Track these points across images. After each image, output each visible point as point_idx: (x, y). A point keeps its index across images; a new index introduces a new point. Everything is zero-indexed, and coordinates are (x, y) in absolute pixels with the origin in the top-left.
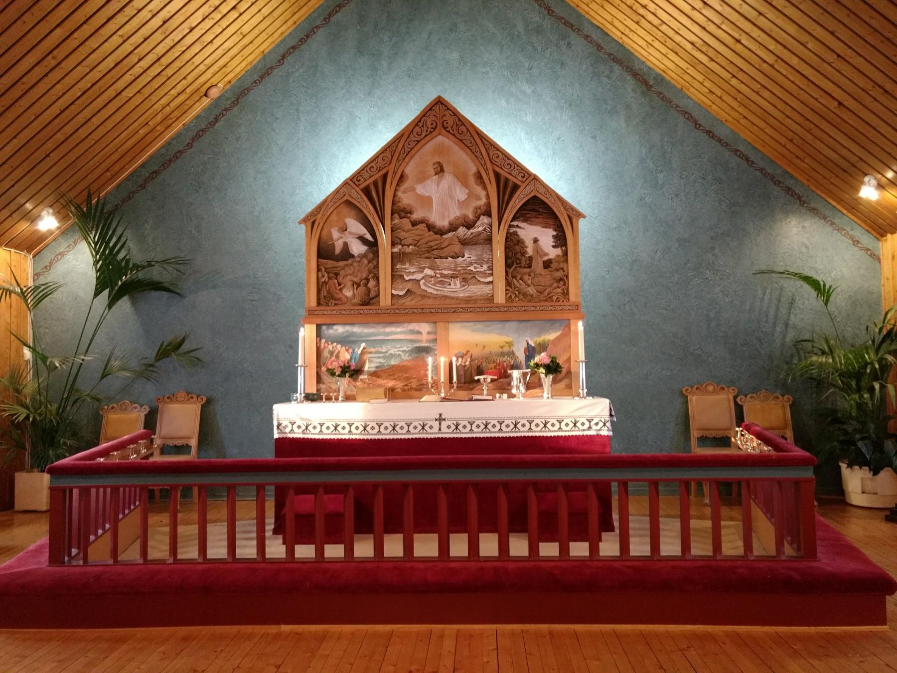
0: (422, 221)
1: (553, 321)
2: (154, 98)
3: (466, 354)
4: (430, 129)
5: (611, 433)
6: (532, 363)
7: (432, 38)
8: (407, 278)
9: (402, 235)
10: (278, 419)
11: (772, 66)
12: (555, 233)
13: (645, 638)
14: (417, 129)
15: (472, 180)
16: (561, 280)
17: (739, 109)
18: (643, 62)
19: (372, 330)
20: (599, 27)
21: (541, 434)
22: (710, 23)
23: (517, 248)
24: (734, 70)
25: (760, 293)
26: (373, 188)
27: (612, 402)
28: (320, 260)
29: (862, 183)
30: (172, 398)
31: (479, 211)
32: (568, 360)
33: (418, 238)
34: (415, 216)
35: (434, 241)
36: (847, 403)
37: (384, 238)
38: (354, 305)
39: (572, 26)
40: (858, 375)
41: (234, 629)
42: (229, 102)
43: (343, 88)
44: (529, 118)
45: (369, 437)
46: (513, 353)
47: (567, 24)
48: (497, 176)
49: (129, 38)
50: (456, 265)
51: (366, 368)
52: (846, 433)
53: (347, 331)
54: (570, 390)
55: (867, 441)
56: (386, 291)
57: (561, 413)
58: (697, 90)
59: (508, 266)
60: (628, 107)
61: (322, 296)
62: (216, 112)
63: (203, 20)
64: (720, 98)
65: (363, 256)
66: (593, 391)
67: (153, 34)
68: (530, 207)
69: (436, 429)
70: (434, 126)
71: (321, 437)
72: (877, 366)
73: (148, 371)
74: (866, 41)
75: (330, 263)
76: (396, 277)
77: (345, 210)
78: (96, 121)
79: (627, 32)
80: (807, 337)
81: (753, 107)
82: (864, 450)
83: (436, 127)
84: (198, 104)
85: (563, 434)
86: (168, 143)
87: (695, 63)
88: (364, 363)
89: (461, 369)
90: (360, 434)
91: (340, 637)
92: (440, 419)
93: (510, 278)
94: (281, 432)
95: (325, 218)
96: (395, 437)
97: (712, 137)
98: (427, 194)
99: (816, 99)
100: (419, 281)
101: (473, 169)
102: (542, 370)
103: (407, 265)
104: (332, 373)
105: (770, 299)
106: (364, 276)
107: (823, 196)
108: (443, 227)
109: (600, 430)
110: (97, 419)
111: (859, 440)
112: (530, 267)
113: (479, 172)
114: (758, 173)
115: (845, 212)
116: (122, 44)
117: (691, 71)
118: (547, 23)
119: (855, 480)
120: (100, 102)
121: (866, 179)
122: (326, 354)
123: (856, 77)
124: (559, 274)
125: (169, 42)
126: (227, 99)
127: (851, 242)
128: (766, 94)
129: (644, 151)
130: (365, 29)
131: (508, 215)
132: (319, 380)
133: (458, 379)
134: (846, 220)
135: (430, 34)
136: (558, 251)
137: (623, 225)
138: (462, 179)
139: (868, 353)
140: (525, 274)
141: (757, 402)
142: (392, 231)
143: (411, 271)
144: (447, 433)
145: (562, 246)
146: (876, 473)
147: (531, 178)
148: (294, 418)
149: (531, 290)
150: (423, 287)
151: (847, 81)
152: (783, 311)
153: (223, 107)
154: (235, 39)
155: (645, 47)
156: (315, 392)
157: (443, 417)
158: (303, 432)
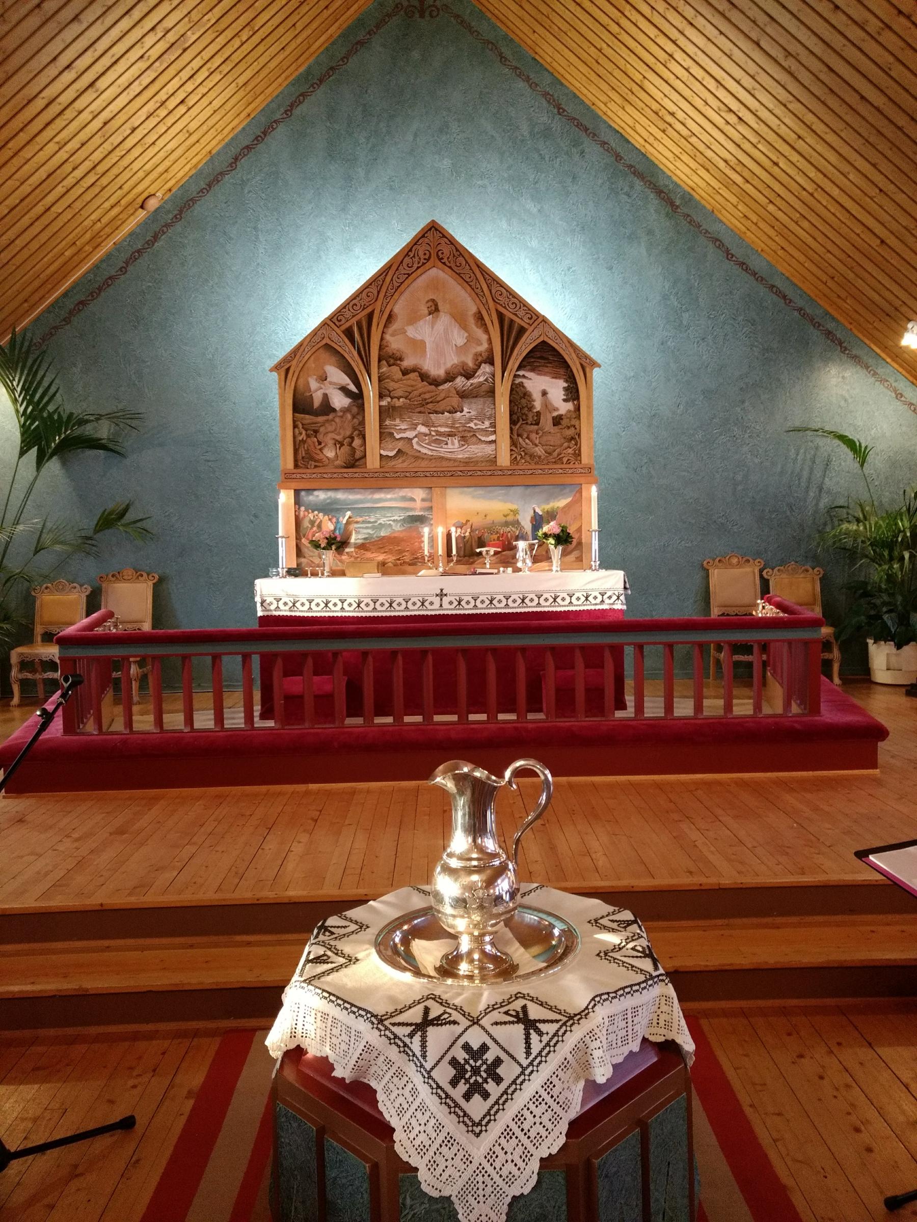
0: (414, 370)
1: (563, 486)
2: (84, 213)
3: (466, 524)
4: (422, 261)
5: (625, 607)
6: (540, 533)
7: (418, 139)
8: (398, 437)
9: (391, 385)
10: (261, 596)
11: (812, 195)
12: (566, 385)
13: (658, 786)
14: (407, 260)
15: (471, 321)
16: (572, 438)
17: (777, 239)
18: (669, 177)
19: (358, 497)
20: (618, 132)
21: (551, 609)
22: (745, 140)
23: (523, 401)
24: (772, 196)
25: (792, 453)
26: (357, 329)
27: (627, 575)
28: (297, 415)
29: (906, 329)
30: (117, 576)
31: (480, 359)
32: (579, 530)
33: (409, 389)
34: (406, 363)
35: (428, 394)
36: (876, 574)
37: (371, 391)
38: (336, 467)
39: (586, 130)
40: (890, 545)
41: (263, 788)
42: (171, 216)
43: (310, 202)
44: (534, 243)
45: (364, 614)
46: (518, 522)
47: (579, 125)
48: (501, 317)
49: (65, 144)
50: (454, 422)
51: (352, 540)
52: (875, 606)
53: (330, 498)
54: (580, 563)
55: (893, 615)
56: (374, 451)
57: (571, 587)
58: (731, 214)
59: (513, 422)
60: (650, 232)
61: (300, 457)
62: (156, 227)
63: (147, 119)
64: (756, 224)
65: (346, 410)
66: (606, 564)
67: (91, 138)
68: (538, 354)
69: (437, 605)
70: (427, 257)
71: (310, 614)
72: (908, 534)
73: (87, 544)
74: (908, 177)
75: (308, 418)
76: (385, 435)
77: (324, 355)
78: (19, 243)
79: (651, 140)
80: (841, 502)
81: (792, 238)
82: (889, 623)
83: (430, 257)
84: (132, 217)
85: (574, 608)
86: (96, 267)
87: (729, 183)
88: (351, 534)
89: (459, 541)
90: (354, 611)
91: (368, 791)
92: (442, 595)
93: (515, 437)
94: (266, 610)
95: (301, 365)
96: (393, 614)
97: (746, 270)
98: (419, 337)
99: (858, 235)
100: (410, 440)
101: (472, 307)
102: (552, 541)
103: (398, 421)
104: (316, 545)
105: (804, 460)
106: (348, 433)
107: (868, 342)
108: (439, 376)
109: (613, 604)
110: (29, 602)
111: (886, 612)
112: (537, 424)
113: (480, 312)
114: (796, 313)
115: (889, 360)
116: (57, 152)
117: (724, 192)
118: (557, 125)
119: (881, 656)
120: (26, 221)
121: (910, 325)
122: (306, 524)
123: (899, 214)
124: (571, 432)
125: (108, 146)
126: (169, 212)
127: (894, 395)
128: (806, 224)
129: (667, 287)
130: (336, 127)
131: (514, 363)
132: (299, 553)
133: (457, 552)
134: (889, 369)
135: (416, 135)
136: (570, 406)
137: (642, 374)
138: (459, 319)
139: (902, 520)
140: (531, 432)
141: (784, 576)
142: (380, 380)
143: (402, 428)
144: (449, 609)
145: (574, 400)
146: (899, 646)
147: (540, 320)
148: (280, 593)
149: (539, 451)
150: (416, 447)
151: (890, 219)
152: (818, 474)
153: (162, 223)
154: (181, 137)
155: (671, 159)
156: (295, 566)
157: (444, 592)
158: (290, 610)
